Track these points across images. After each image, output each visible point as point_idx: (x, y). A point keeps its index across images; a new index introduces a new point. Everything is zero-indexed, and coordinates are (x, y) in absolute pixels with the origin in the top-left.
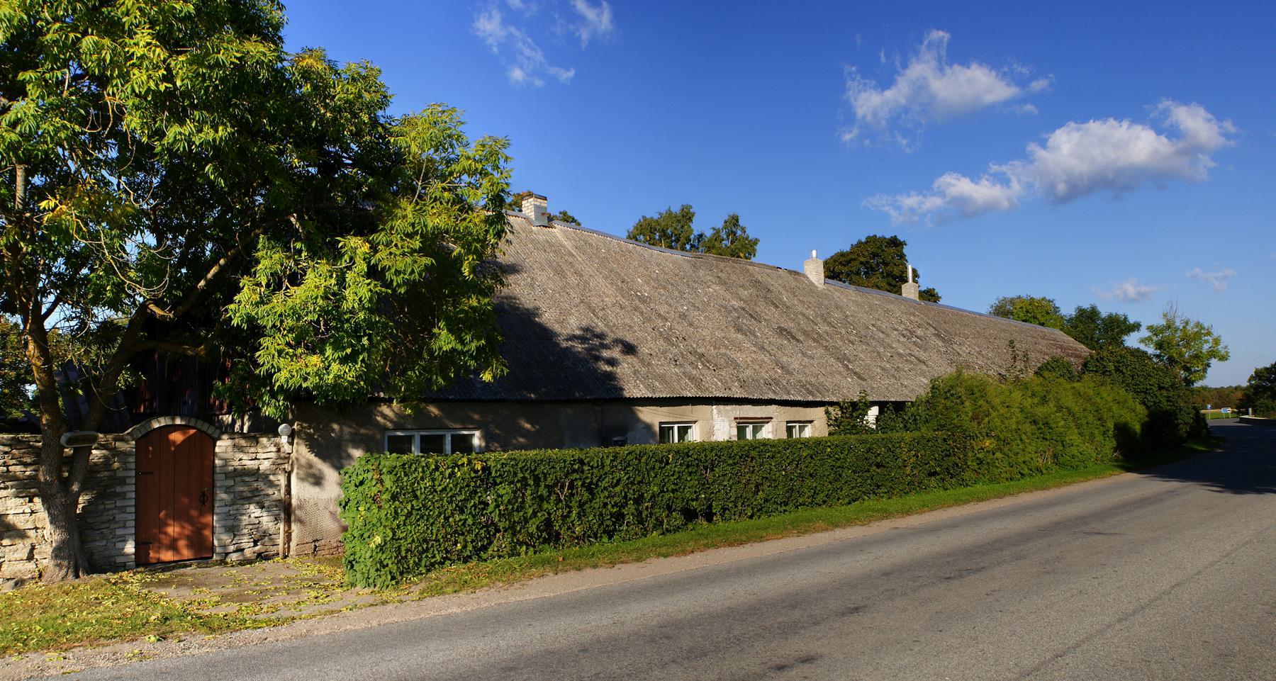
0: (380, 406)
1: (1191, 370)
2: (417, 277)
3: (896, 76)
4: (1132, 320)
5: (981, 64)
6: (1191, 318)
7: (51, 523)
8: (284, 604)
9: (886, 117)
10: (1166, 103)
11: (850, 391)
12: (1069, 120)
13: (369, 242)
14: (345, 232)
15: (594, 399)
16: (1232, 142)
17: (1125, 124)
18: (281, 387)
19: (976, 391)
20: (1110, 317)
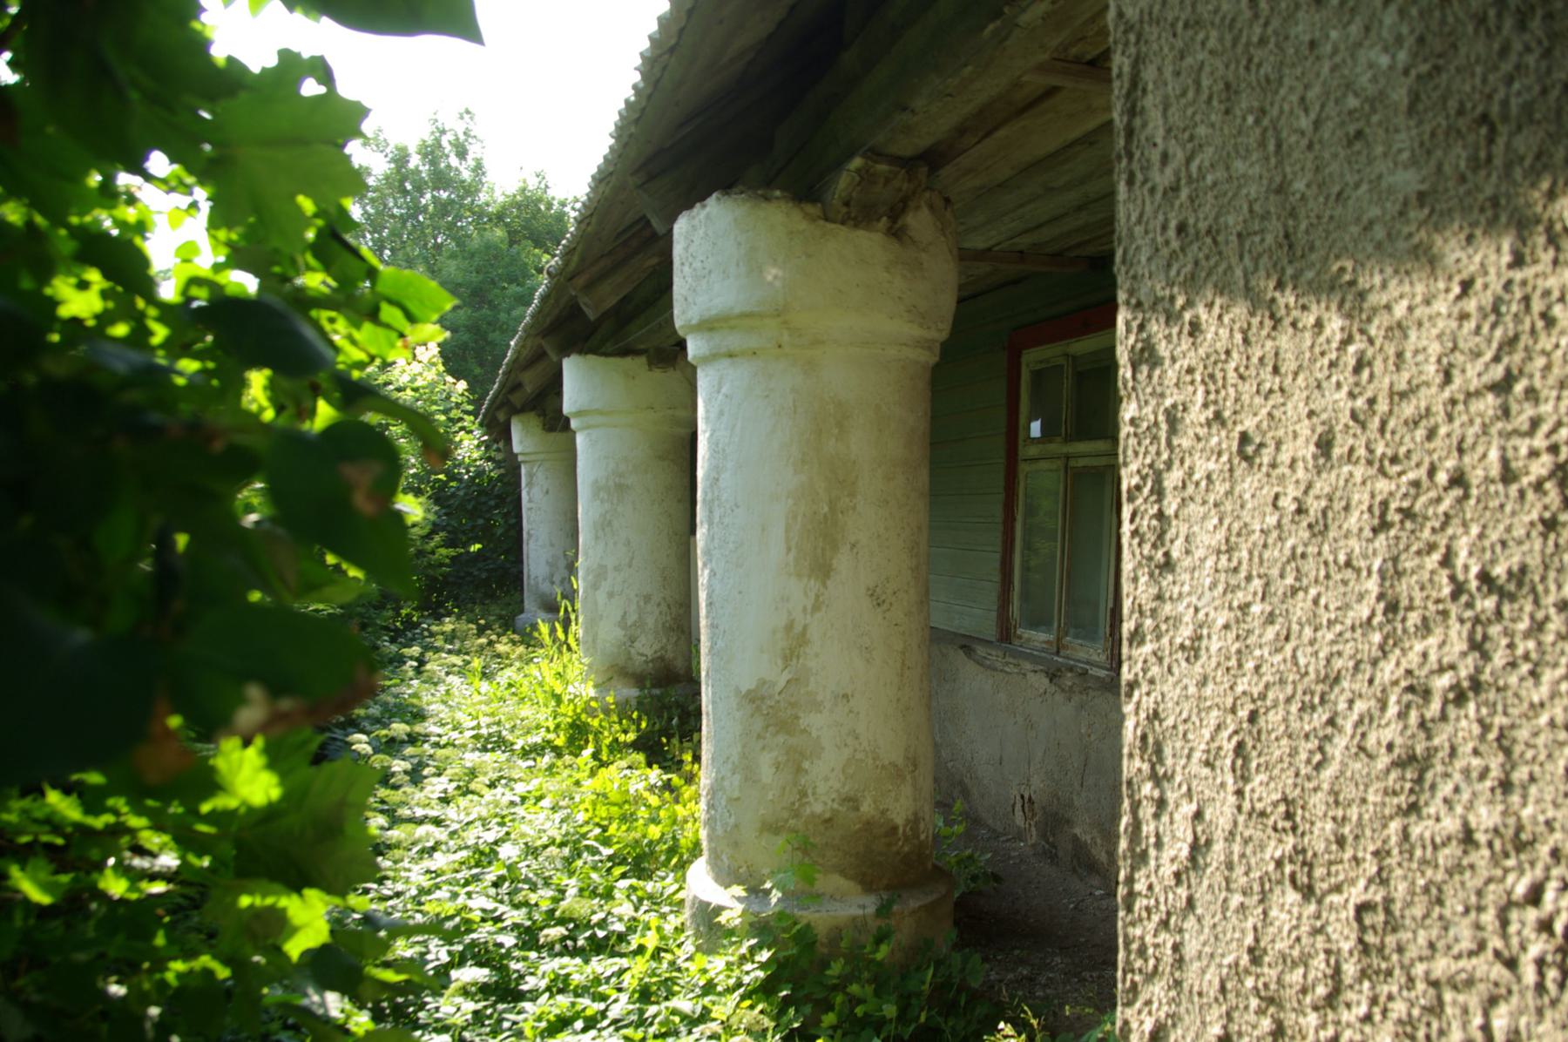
0: (363, 294)
1: (645, 854)
2: (1393, 283)
3: (211, 762)
4: (828, 582)
5: (201, 45)
6: (402, 142)
7: (854, 919)
8: (1185, 735)
9: (222, 259)
10: (237, 503)
11: (373, 351)
12: (352, 168)
13: (832, 505)
14: (54, 787)
15: (1168, 421)
16: (75, 777)
17: (637, 77)
18: (247, 743)
19: (329, 913)
20: (313, 58)
